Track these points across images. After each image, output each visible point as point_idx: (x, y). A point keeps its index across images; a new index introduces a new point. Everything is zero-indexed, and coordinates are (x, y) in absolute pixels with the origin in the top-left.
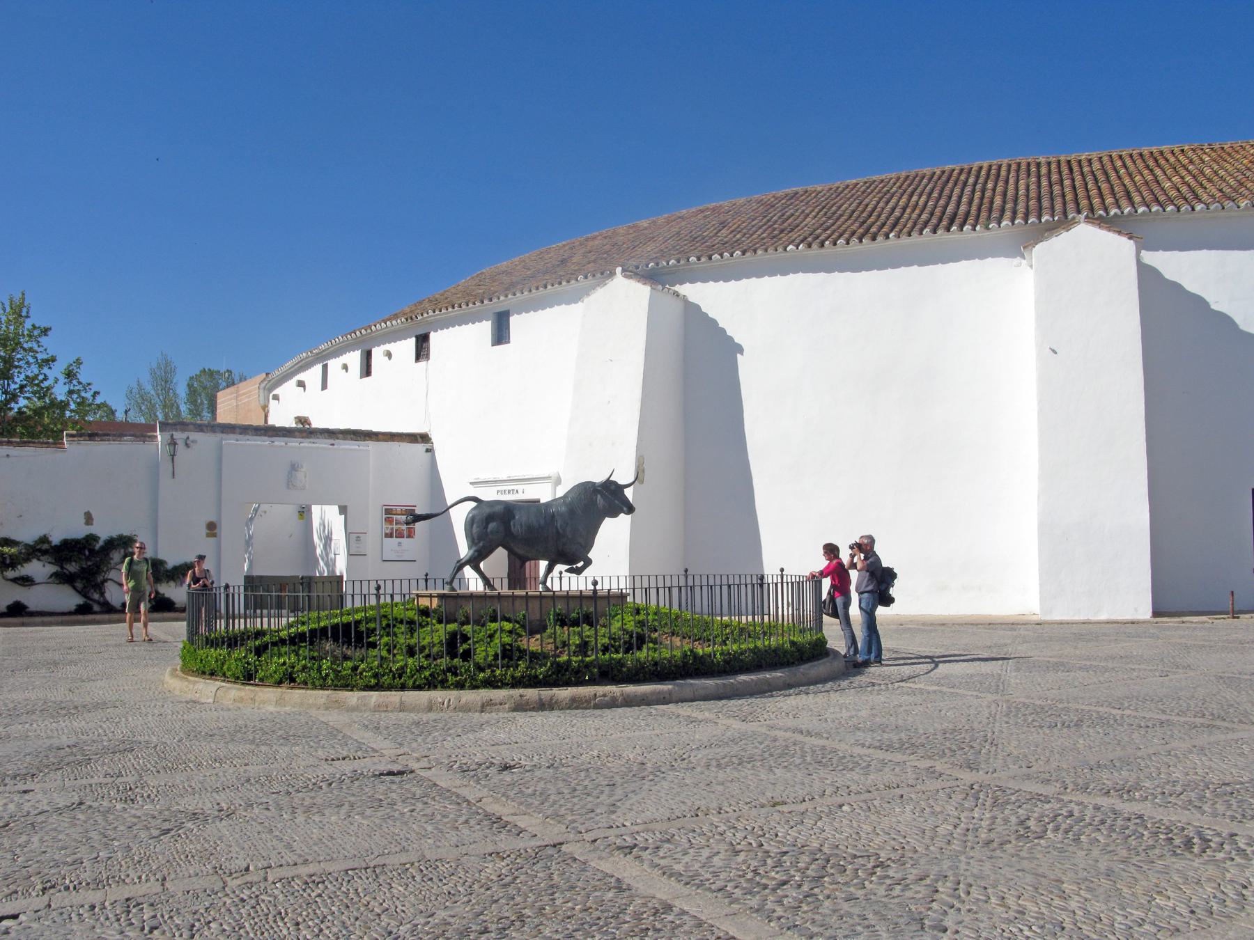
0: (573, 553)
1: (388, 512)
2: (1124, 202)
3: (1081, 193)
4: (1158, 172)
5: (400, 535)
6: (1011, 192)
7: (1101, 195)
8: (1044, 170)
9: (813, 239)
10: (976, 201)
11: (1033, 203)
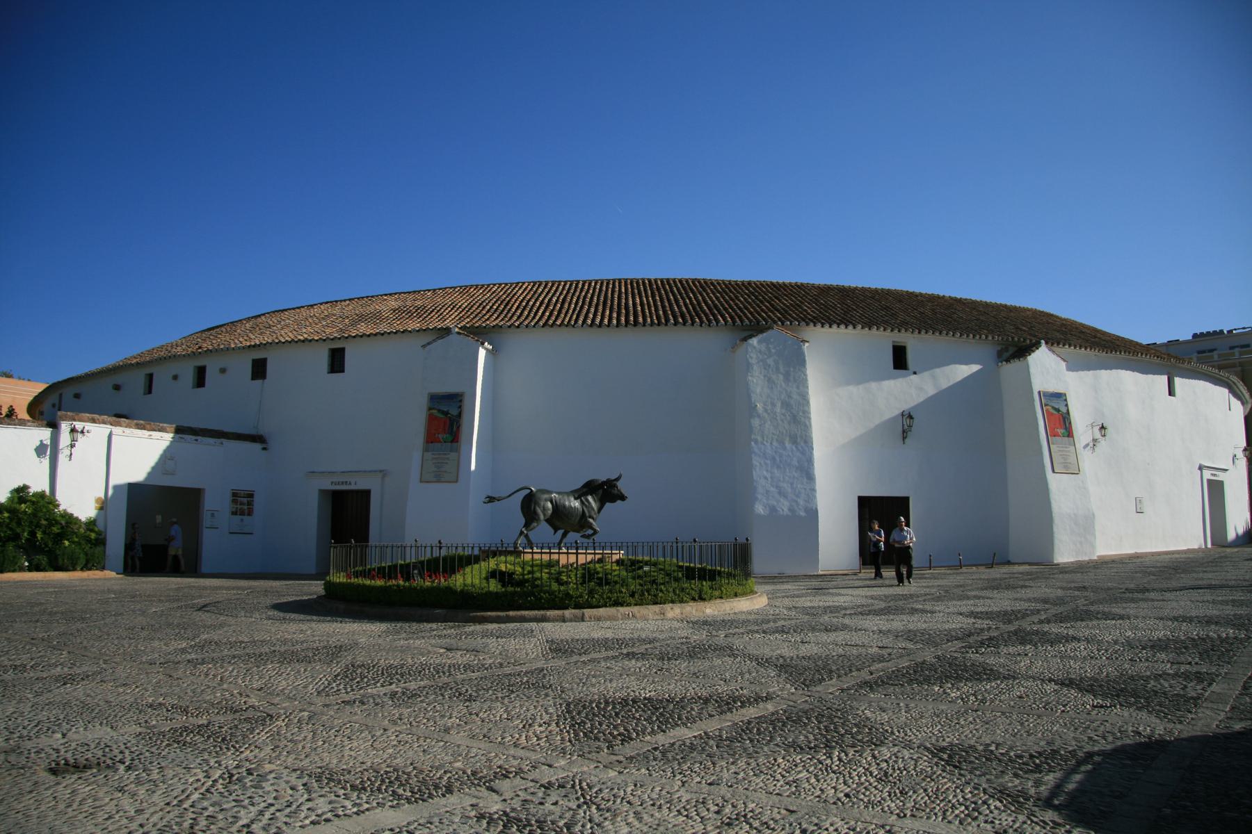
5: (242, 513)
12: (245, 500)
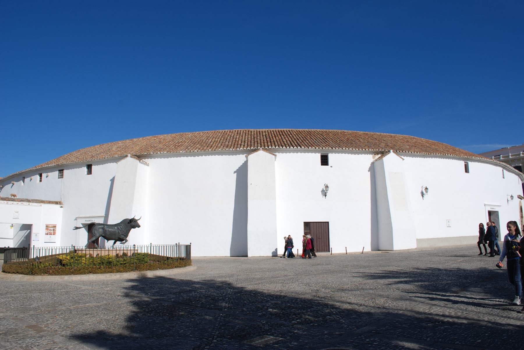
0: (122, 238)
1: (47, 226)
2: (273, 144)
3: (262, 141)
4: (282, 136)
5: (51, 234)
6: (243, 139)
7: (267, 142)
8: (253, 133)
9: (421, 150)
10: (234, 142)
11: (249, 143)
12: (52, 229)
